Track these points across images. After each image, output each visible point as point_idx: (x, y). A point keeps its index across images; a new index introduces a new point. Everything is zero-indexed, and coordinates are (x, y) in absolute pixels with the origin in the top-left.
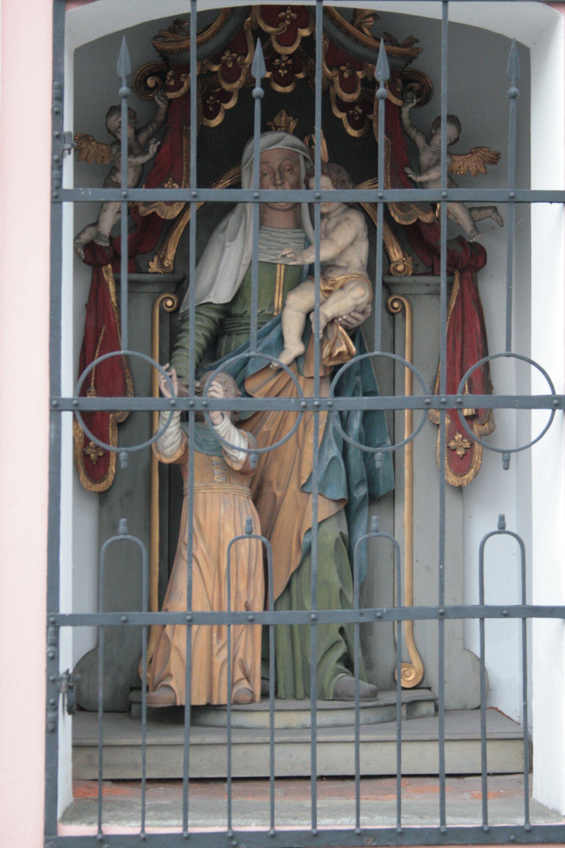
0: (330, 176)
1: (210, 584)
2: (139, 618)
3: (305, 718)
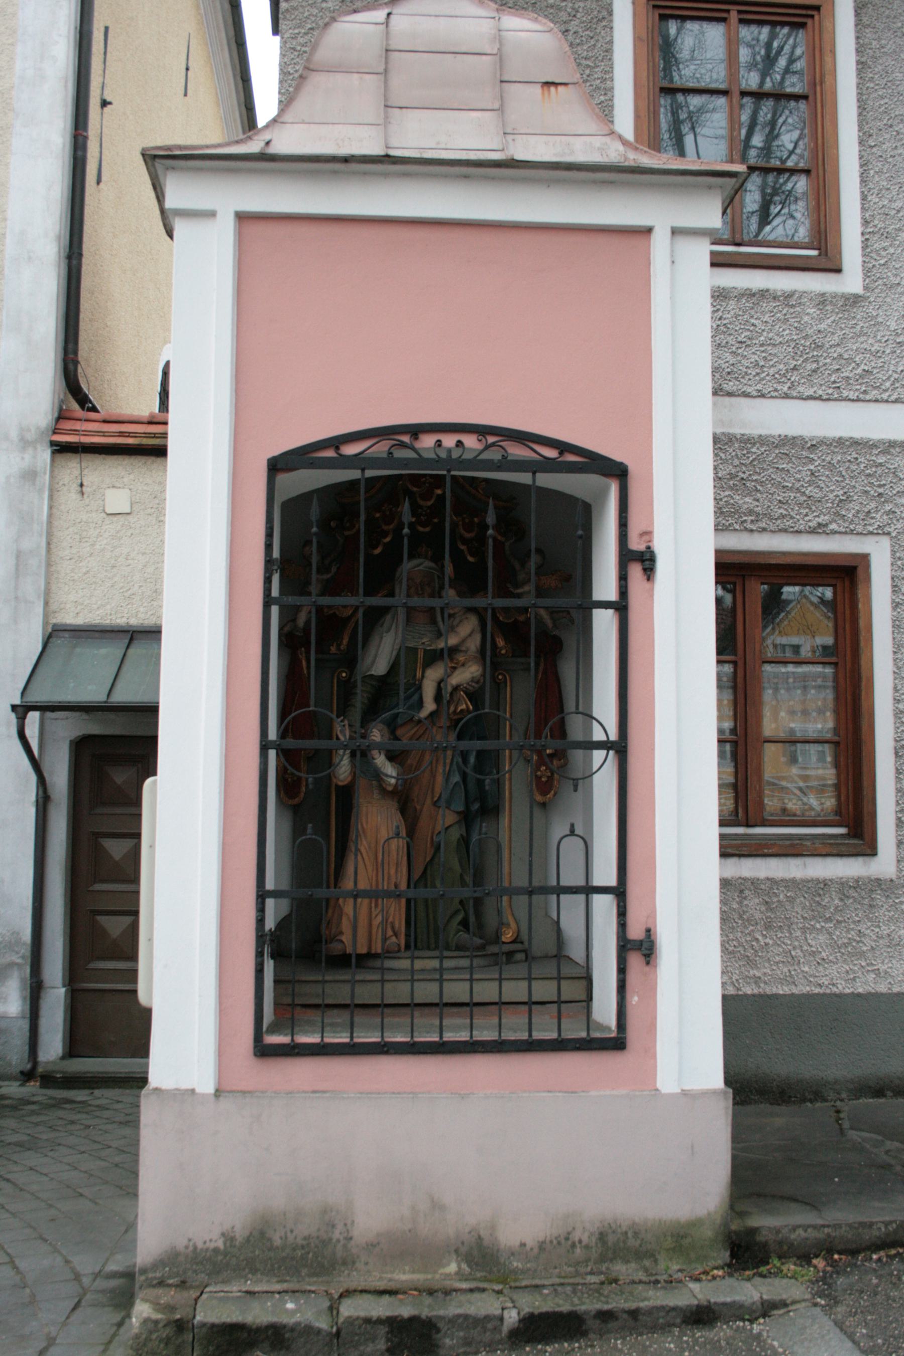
0: (455, 589)
2: (321, 893)
3: (435, 963)
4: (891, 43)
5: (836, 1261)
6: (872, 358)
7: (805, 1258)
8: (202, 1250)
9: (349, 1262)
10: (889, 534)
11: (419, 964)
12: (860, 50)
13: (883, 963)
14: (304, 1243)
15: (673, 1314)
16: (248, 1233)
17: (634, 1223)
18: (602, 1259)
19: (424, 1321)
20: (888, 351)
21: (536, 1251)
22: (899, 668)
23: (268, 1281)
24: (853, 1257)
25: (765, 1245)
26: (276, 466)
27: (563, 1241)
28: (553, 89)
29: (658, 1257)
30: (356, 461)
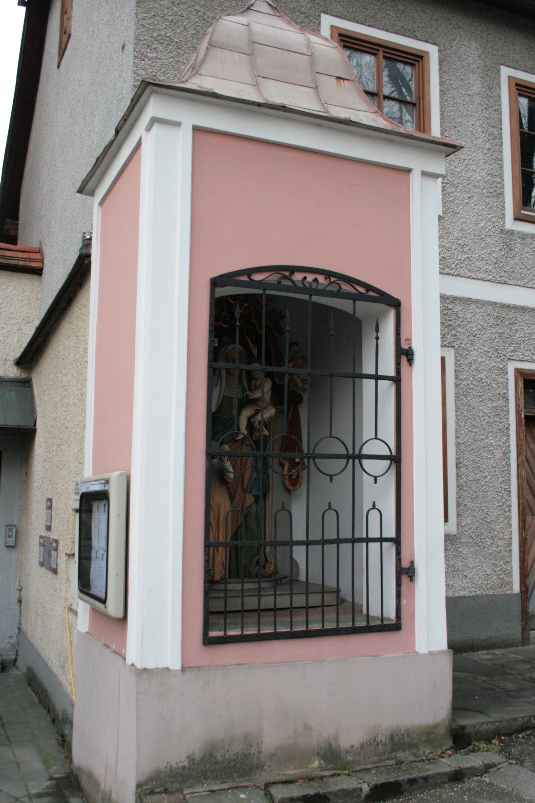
1: (214, 531)
3: (256, 586)
4: (456, 82)
5: (503, 740)
6: (446, 251)
7: (488, 740)
8: (175, 768)
9: (260, 767)
10: (454, 347)
11: (247, 586)
12: (441, 84)
13: (450, 580)
14: (235, 757)
15: (444, 776)
16: (202, 755)
17: (407, 729)
18: (392, 751)
19: (321, 796)
20: (453, 248)
21: (359, 749)
22: (458, 420)
23: (215, 783)
24: (510, 737)
25: (469, 735)
26: (215, 283)
27: (373, 742)
28: (341, 81)
29: (419, 746)
30: (259, 284)
